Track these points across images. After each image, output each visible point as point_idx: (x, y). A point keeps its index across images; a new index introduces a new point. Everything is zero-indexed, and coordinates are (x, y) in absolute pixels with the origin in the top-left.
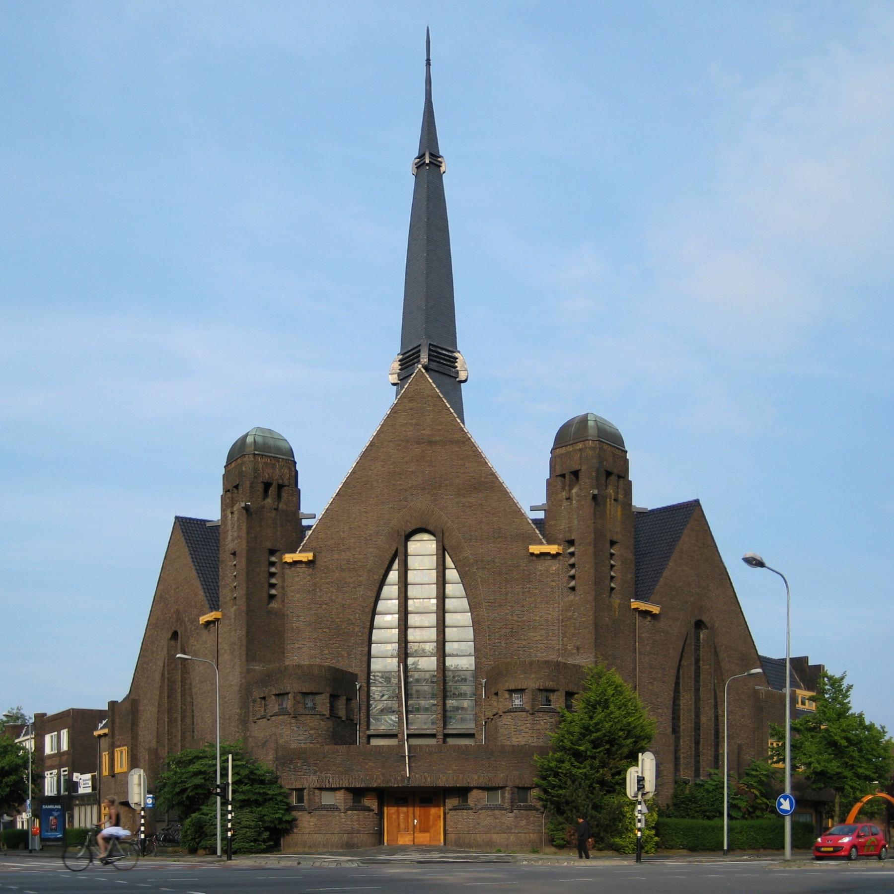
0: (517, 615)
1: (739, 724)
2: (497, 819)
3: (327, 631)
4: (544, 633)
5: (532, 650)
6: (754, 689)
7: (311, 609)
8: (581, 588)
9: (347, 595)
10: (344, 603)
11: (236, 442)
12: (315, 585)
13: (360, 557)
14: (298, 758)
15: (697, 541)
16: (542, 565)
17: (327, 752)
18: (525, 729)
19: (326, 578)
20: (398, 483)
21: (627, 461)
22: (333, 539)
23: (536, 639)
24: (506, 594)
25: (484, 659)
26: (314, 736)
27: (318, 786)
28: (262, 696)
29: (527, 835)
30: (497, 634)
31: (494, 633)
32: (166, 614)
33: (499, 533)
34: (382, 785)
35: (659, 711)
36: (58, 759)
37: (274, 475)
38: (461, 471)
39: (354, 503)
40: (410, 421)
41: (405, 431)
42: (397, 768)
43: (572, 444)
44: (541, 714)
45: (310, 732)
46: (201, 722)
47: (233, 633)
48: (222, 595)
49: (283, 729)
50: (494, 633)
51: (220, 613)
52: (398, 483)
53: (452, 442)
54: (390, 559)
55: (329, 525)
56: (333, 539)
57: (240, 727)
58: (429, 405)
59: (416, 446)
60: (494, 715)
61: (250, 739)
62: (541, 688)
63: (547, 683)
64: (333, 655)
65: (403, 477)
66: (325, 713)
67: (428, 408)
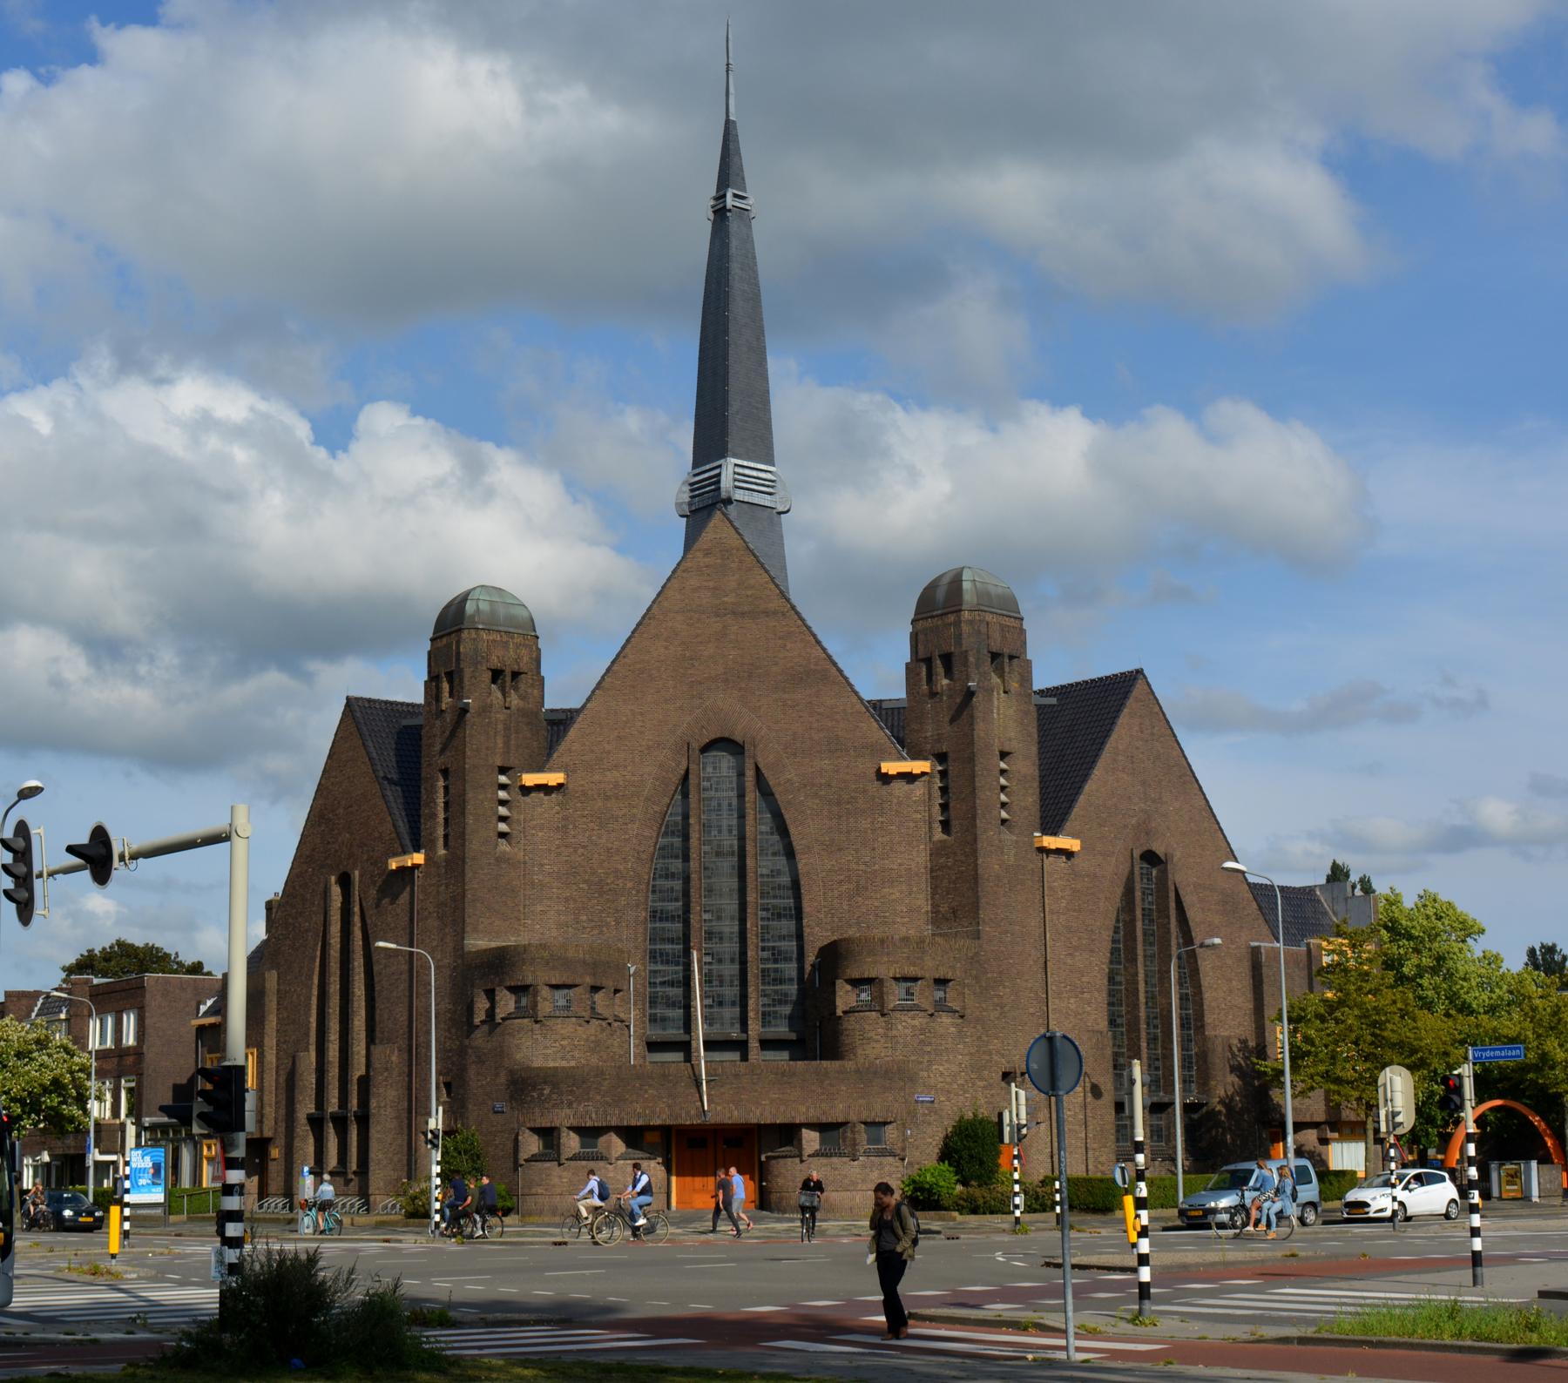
0: (865, 863)
1: (1223, 1006)
2: (836, 1169)
5: (887, 914)
6: (951, 680)
7: (559, 854)
9: (614, 834)
10: (610, 845)
12: (565, 818)
14: (545, 1083)
15: (1142, 732)
16: (899, 787)
20: (690, 672)
21: (1022, 632)
22: (592, 751)
23: (894, 897)
24: (848, 832)
25: (817, 929)
26: (568, 1049)
31: (832, 890)
32: (329, 843)
33: (837, 744)
34: (668, 1122)
36: (115, 1060)
37: (506, 659)
40: (706, 584)
43: (942, 615)
44: (898, 1014)
47: (443, 887)
49: (520, 1039)
50: (832, 890)
52: (690, 672)
53: (766, 613)
55: (587, 732)
56: (592, 751)
57: (453, 1031)
59: (714, 619)
61: (470, 1051)
62: (898, 976)
64: (593, 924)
65: (696, 664)
66: (584, 1014)
67: (732, 565)
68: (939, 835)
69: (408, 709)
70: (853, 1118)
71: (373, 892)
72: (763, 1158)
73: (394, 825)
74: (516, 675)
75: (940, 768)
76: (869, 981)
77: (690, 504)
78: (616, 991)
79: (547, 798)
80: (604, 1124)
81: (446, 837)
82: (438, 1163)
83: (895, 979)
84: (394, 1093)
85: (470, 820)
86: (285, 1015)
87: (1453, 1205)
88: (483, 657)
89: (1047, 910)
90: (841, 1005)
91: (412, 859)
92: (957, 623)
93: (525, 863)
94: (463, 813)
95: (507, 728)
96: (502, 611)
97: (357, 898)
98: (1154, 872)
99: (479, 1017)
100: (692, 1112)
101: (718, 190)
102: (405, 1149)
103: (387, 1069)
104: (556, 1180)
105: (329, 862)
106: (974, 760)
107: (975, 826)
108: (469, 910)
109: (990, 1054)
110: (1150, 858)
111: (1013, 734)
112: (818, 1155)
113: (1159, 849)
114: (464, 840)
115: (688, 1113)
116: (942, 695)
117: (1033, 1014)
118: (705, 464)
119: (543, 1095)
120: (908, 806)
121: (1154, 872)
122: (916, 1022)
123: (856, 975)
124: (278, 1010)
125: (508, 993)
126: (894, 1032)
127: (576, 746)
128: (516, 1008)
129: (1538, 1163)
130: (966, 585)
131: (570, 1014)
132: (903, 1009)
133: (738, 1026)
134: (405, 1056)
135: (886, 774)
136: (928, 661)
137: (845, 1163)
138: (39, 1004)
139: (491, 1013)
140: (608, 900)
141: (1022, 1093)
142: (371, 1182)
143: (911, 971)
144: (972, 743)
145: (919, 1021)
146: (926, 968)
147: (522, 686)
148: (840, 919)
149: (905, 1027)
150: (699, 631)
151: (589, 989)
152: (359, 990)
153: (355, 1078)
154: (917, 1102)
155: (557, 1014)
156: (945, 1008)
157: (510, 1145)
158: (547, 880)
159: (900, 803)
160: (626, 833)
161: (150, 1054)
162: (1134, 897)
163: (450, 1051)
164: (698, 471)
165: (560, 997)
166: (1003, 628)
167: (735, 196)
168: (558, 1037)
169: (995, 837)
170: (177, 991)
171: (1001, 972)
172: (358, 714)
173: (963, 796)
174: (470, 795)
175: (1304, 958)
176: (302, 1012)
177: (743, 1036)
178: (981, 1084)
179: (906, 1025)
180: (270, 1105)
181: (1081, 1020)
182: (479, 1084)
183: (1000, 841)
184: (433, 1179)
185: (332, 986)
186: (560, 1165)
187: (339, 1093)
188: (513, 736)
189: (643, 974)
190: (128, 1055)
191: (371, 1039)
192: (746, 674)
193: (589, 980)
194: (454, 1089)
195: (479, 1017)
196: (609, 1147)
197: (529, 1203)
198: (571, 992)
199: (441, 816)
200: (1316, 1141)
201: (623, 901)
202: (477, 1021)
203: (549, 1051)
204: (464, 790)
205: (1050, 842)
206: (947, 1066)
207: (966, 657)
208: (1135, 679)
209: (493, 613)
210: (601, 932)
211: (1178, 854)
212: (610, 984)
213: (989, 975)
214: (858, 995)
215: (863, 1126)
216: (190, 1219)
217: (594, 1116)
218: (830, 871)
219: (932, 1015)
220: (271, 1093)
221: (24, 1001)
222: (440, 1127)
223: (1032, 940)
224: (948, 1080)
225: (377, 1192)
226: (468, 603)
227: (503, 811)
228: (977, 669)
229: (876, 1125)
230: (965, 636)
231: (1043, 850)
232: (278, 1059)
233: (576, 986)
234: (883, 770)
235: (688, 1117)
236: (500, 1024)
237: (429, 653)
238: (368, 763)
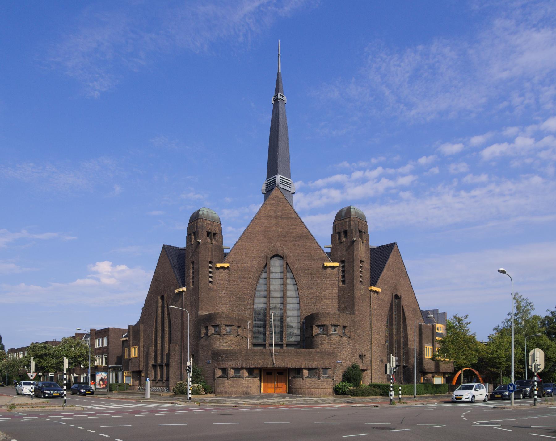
0: (319, 293)
3: (235, 298)
4: (330, 300)
5: (325, 308)
6: (347, 238)
7: (227, 288)
8: (348, 281)
10: (243, 286)
11: (193, 214)
12: (229, 277)
14: (224, 354)
16: (329, 271)
19: (235, 275)
21: (367, 226)
22: (238, 258)
23: (327, 303)
26: (230, 344)
27: (233, 367)
28: (206, 326)
29: (327, 389)
32: (158, 287)
35: (380, 334)
36: (102, 350)
37: (212, 229)
38: (295, 231)
40: (273, 209)
41: (270, 213)
42: (269, 359)
43: (344, 219)
44: (332, 336)
45: (229, 342)
46: (175, 337)
47: (192, 297)
48: (187, 280)
51: (186, 288)
53: (291, 218)
57: (195, 339)
58: (281, 202)
59: (275, 219)
60: (310, 336)
61: (200, 345)
63: (335, 322)
66: (235, 334)
67: (280, 203)
68: (341, 285)
69: (182, 250)
70: (319, 366)
71: (171, 300)
72: (290, 378)
73: (177, 280)
74: (215, 234)
75: (342, 265)
76: (323, 326)
77: (266, 190)
78: (245, 328)
79: (224, 271)
80: (242, 367)
81: (193, 282)
82: (190, 377)
83: (332, 325)
84: (177, 358)
85: (200, 276)
86: (146, 337)
87: (487, 397)
88: (204, 228)
89: (372, 308)
90: (314, 333)
91: (182, 289)
92: (349, 221)
93: (217, 290)
94: (198, 274)
95: (212, 250)
96: (210, 215)
97: (166, 302)
98: (397, 301)
99: (203, 335)
100: (270, 364)
101: (275, 93)
102: (180, 374)
104: (227, 384)
105: (158, 293)
106: (354, 262)
107: (353, 282)
108: (200, 303)
109: (357, 349)
110: (397, 297)
111: (364, 256)
112: (308, 378)
113: (399, 295)
114: (199, 282)
115: (268, 364)
116: (343, 243)
117: (367, 338)
118: (271, 177)
119: (223, 358)
121: (397, 301)
122: (337, 339)
123: (319, 324)
124: (144, 335)
126: (331, 341)
127: (233, 256)
128: (214, 332)
129: (489, 384)
130: (352, 210)
131: (231, 334)
132: (334, 335)
133: (280, 340)
134: (180, 347)
135: (326, 266)
136: (339, 233)
137: (316, 380)
138: (84, 336)
139: (206, 334)
140: (242, 302)
141: (394, 358)
142: (170, 383)
143: (337, 323)
144: (353, 257)
145: (338, 338)
146: (340, 322)
147: (217, 238)
148: (311, 309)
149: (334, 340)
150: (270, 223)
151: (237, 327)
152: (167, 329)
153: (165, 354)
154: (337, 362)
155: (227, 334)
156: (345, 335)
157: (212, 373)
159: (329, 275)
161: (111, 349)
162: (393, 307)
163: (194, 345)
164: (268, 180)
165: (228, 329)
166: (362, 224)
167: (281, 95)
168: (227, 341)
169: (359, 285)
170: (118, 332)
171: (360, 326)
172: (167, 249)
173: (350, 272)
174: (200, 269)
175: (431, 328)
176: (150, 336)
177: (282, 343)
178: (354, 358)
179: (335, 339)
180: (142, 362)
181: (379, 341)
182: (203, 355)
183: (360, 287)
184: (189, 383)
185: (159, 328)
186: (228, 379)
187: (161, 358)
188: (214, 253)
189: (252, 324)
190: (105, 349)
191: (170, 342)
193: (237, 324)
194: (194, 357)
195: (203, 335)
196: (243, 374)
197: (218, 390)
198: (231, 327)
199: (191, 276)
200: (431, 377)
201: (246, 302)
202: (202, 336)
203: (225, 345)
204: (199, 267)
205: (373, 288)
206: (345, 352)
207: (352, 231)
208: (394, 245)
209: (208, 215)
210: (240, 311)
211: (403, 296)
212: (242, 325)
213: (357, 326)
214: (319, 330)
215: (322, 369)
216: (119, 392)
217: (239, 364)
219: (342, 337)
220: (142, 358)
221: (80, 336)
222: (191, 365)
223: (368, 317)
224: (346, 356)
226: (200, 211)
227: (210, 275)
228: (355, 235)
229: (326, 369)
230: (352, 225)
231: (371, 291)
232: (144, 349)
233: (234, 325)
234: (325, 265)
235: (268, 365)
236: (209, 337)
237: (188, 228)
238: (170, 263)
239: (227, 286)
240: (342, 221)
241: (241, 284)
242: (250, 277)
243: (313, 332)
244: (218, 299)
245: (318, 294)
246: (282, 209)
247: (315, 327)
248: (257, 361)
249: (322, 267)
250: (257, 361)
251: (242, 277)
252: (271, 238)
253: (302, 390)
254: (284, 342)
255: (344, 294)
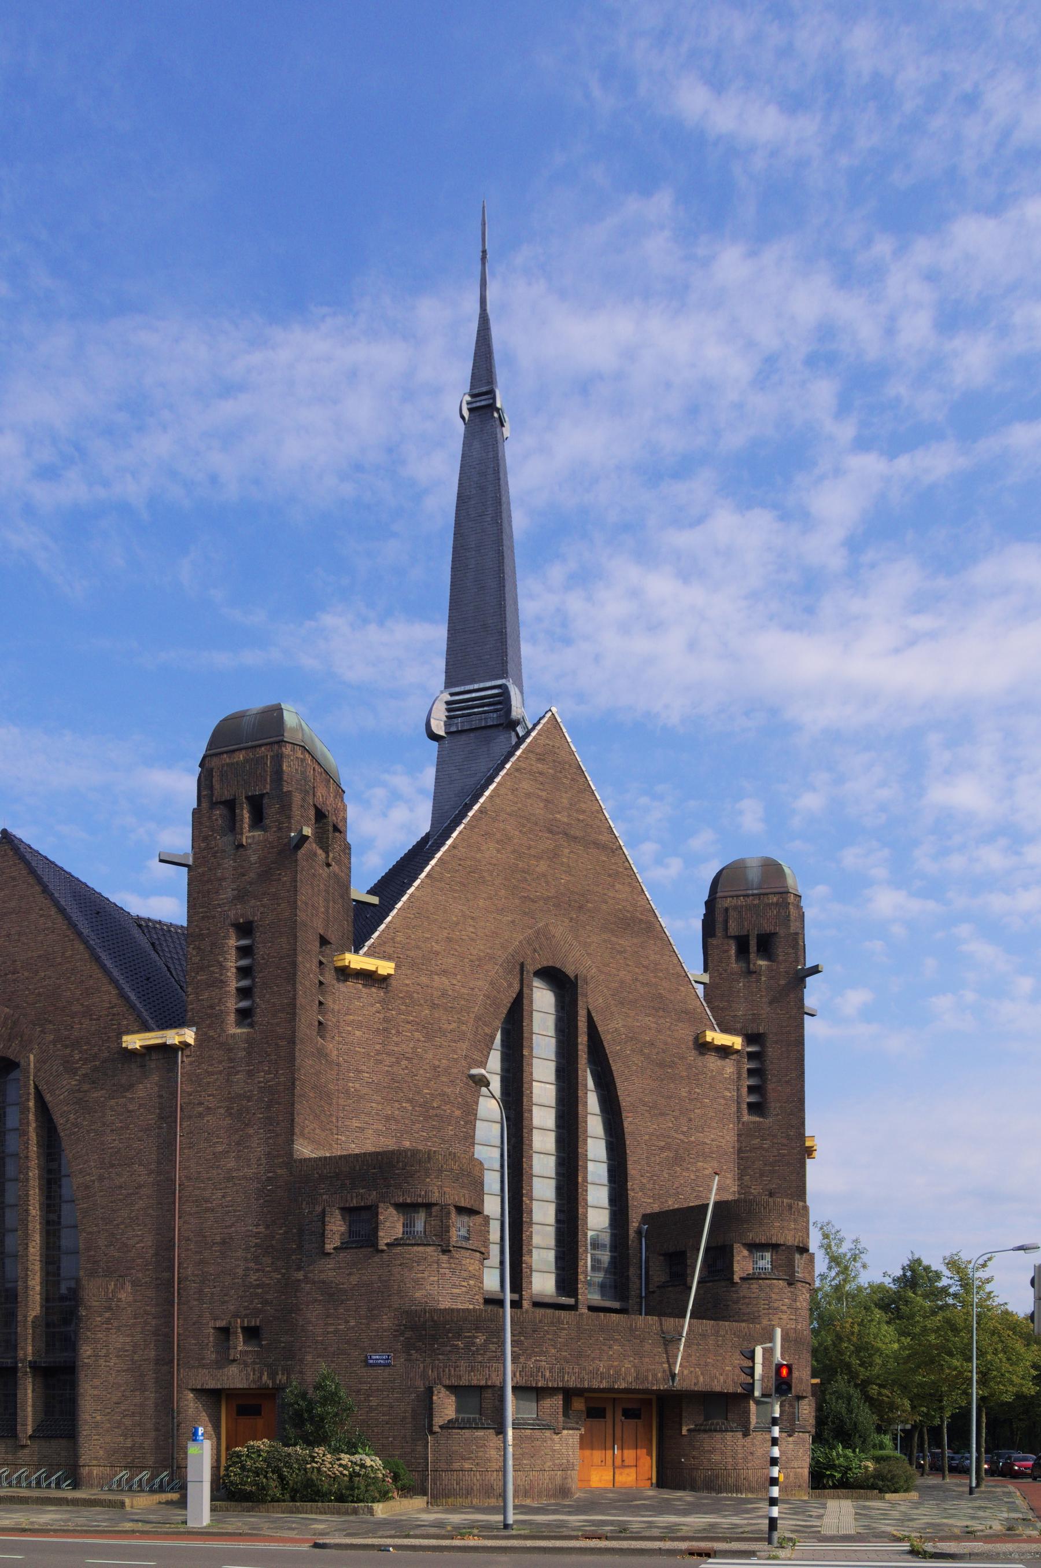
5: (701, 1189)
6: (251, 1025)
7: (381, 1062)
8: (778, 1105)
10: (437, 1063)
12: (386, 1020)
13: (463, 990)
14: (477, 1329)
16: (712, 1062)
17: (540, 1322)
18: (782, 1307)
19: (409, 1014)
22: (418, 947)
25: (640, 1194)
30: (657, 1157)
39: (455, 898)
41: (531, 805)
53: (597, 845)
54: (509, 1005)
58: (566, 777)
67: (565, 781)
76: (774, 1247)
79: (365, 990)
93: (338, 1065)
103: (109, 1309)
119: (473, 1344)
120: (720, 1082)
125: (395, 1212)
153: (30, 1319)
158: (364, 1091)
160: (455, 1052)
168: (465, 1274)
192: (577, 905)
202: (329, 1247)
203: (457, 1291)
217: (547, 1374)
218: (652, 1134)
225: (95, 1462)
230: (792, 918)
239: (378, 1053)
240: (749, 900)
241: (430, 1056)
242: (464, 1033)
243: (736, 1267)
244: (341, 1102)
245: (681, 1137)
246: (571, 804)
247: (742, 1248)
248: (616, 1363)
249: (691, 1044)
250: (616, 1363)
251: (436, 1027)
252: (533, 901)
253: (738, 1475)
254: (580, 1297)
255: (761, 1148)
